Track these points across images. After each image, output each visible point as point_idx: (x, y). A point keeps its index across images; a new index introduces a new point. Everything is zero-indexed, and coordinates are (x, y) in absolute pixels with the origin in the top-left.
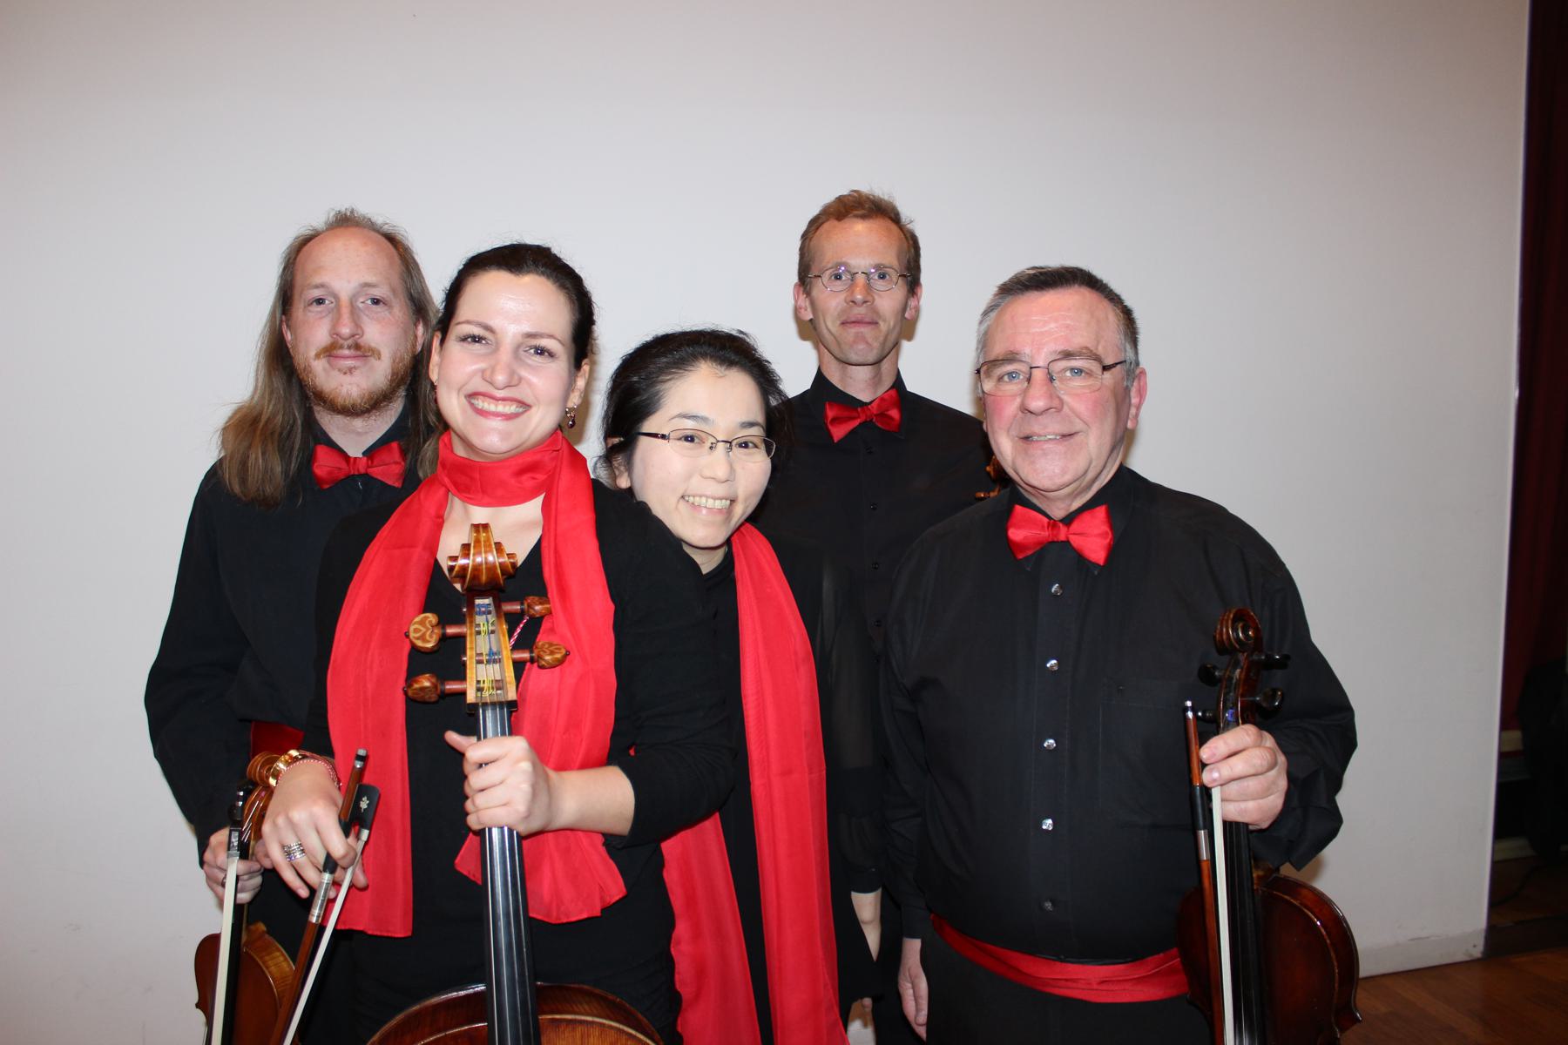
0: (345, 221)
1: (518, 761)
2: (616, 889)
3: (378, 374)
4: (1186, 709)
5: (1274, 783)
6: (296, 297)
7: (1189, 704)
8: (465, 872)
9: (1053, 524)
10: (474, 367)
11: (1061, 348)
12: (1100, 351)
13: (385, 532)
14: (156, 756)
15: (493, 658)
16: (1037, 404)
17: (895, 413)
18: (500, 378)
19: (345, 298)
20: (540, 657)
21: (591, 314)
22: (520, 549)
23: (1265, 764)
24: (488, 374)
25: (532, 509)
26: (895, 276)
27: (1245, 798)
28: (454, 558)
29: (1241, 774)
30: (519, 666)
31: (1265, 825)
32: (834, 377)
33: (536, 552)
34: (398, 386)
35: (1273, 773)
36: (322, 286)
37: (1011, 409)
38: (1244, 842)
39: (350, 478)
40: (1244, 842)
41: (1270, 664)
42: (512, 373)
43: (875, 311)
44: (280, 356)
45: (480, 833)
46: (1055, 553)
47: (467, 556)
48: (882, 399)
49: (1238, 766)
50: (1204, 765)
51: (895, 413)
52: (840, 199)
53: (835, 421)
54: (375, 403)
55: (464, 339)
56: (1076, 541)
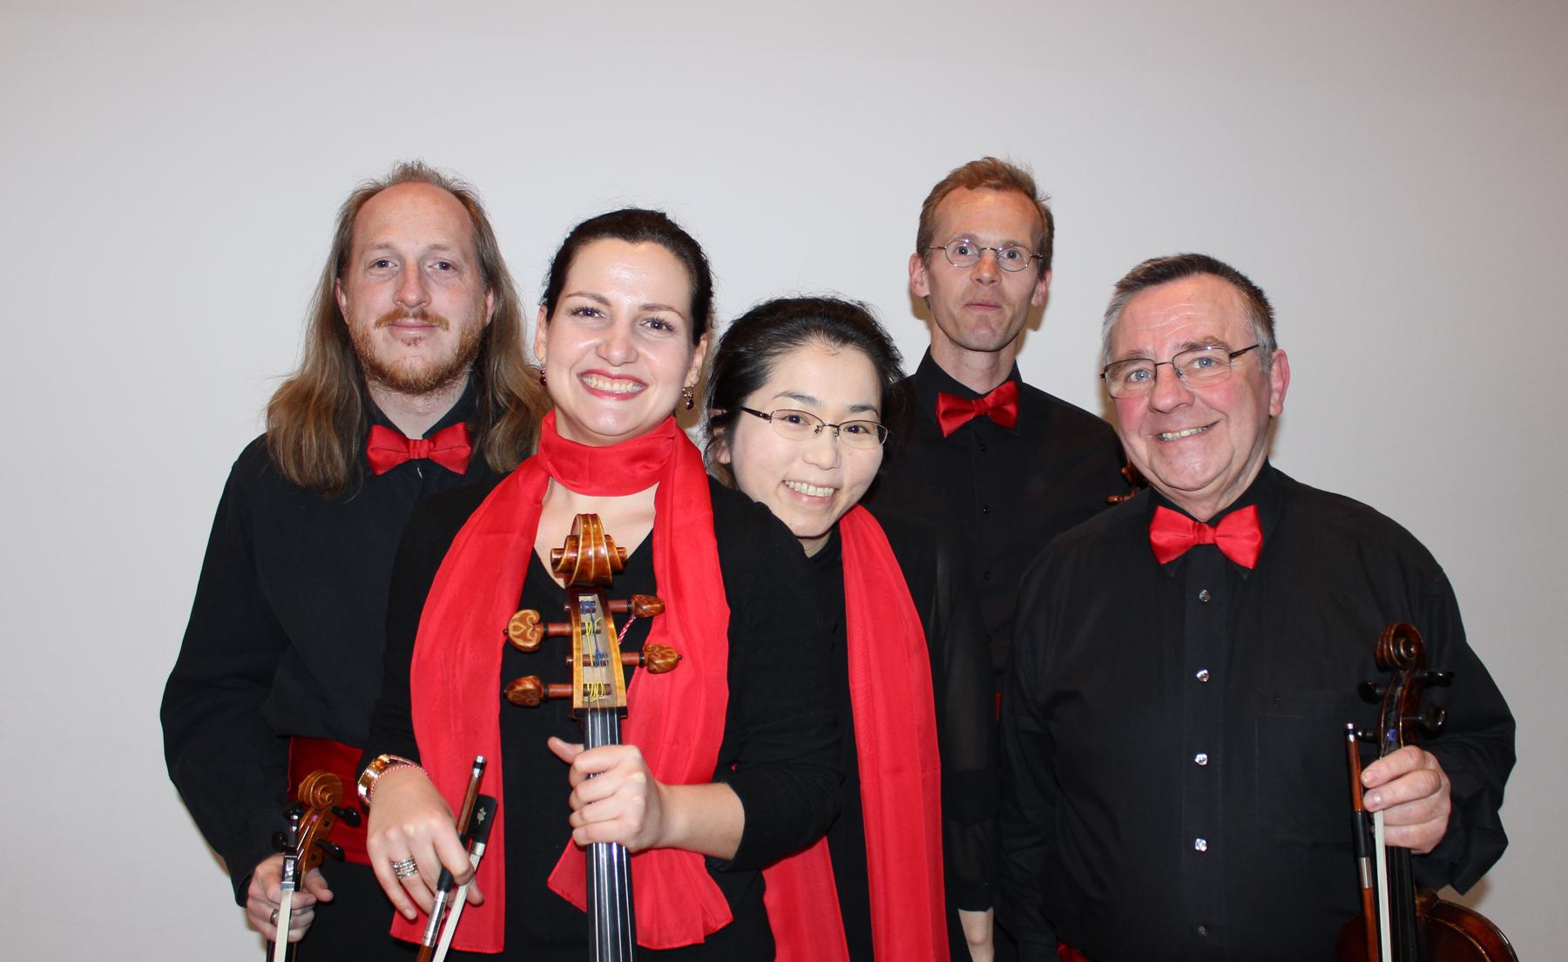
0: (411, 176)
1: (631, 772)
2: (721, 915)
3: (446, 345)
4: (1347, 732)
5: (1437, 806)
6: (355, 258)
7: (1350, 726)
8: (558, 892)
9: (1198, 525)
10: (583, 345)
11: (1183, 341)
12: (1227, 338)
13: (478, 518)
14: (172, 778)
15: (600, 660)
16: (1165, 402)
17: (1011, 408)
18: (617, 354)
19: (411, 261)
20: (651, 660)
21: (709, 284)
22: (630, 540)
23: (1429, 788)
24: (603, 349)
25: (645, 500)
26: (1026, 256)
27: (1407, 821)
28: (561, 551)
29: (1403, 796)
30: (628, 669)
31: (1428, 850)
32: (947, 362)
33: (647, 546)
34: (465, 361)
35: (1437, 795)
36: (387, 246)
37: (1140, 408)
38: (1405, 868)
39: (410, 464)
40: (1405, 868)
41: (1432, 681)
42: (630, 349)
43: (1001, 293)
44: (333, 325)
45: (586, 850)
46: (1204, 557)
47: (576, 548)
48: (998, 391)
49: (1401, 789)
50: (1366, 790)
51: (1011, 408)
52: (972, 166)
53: (948, 414)
54: (439, 380)
55: (575, 313)
56: (1224, 544)
